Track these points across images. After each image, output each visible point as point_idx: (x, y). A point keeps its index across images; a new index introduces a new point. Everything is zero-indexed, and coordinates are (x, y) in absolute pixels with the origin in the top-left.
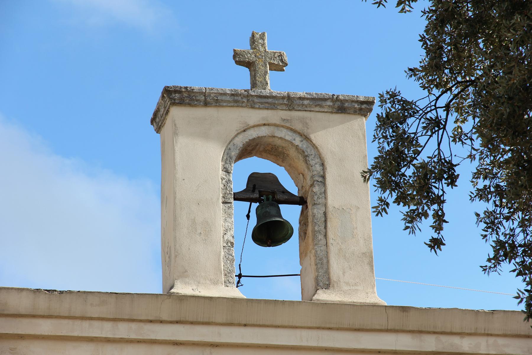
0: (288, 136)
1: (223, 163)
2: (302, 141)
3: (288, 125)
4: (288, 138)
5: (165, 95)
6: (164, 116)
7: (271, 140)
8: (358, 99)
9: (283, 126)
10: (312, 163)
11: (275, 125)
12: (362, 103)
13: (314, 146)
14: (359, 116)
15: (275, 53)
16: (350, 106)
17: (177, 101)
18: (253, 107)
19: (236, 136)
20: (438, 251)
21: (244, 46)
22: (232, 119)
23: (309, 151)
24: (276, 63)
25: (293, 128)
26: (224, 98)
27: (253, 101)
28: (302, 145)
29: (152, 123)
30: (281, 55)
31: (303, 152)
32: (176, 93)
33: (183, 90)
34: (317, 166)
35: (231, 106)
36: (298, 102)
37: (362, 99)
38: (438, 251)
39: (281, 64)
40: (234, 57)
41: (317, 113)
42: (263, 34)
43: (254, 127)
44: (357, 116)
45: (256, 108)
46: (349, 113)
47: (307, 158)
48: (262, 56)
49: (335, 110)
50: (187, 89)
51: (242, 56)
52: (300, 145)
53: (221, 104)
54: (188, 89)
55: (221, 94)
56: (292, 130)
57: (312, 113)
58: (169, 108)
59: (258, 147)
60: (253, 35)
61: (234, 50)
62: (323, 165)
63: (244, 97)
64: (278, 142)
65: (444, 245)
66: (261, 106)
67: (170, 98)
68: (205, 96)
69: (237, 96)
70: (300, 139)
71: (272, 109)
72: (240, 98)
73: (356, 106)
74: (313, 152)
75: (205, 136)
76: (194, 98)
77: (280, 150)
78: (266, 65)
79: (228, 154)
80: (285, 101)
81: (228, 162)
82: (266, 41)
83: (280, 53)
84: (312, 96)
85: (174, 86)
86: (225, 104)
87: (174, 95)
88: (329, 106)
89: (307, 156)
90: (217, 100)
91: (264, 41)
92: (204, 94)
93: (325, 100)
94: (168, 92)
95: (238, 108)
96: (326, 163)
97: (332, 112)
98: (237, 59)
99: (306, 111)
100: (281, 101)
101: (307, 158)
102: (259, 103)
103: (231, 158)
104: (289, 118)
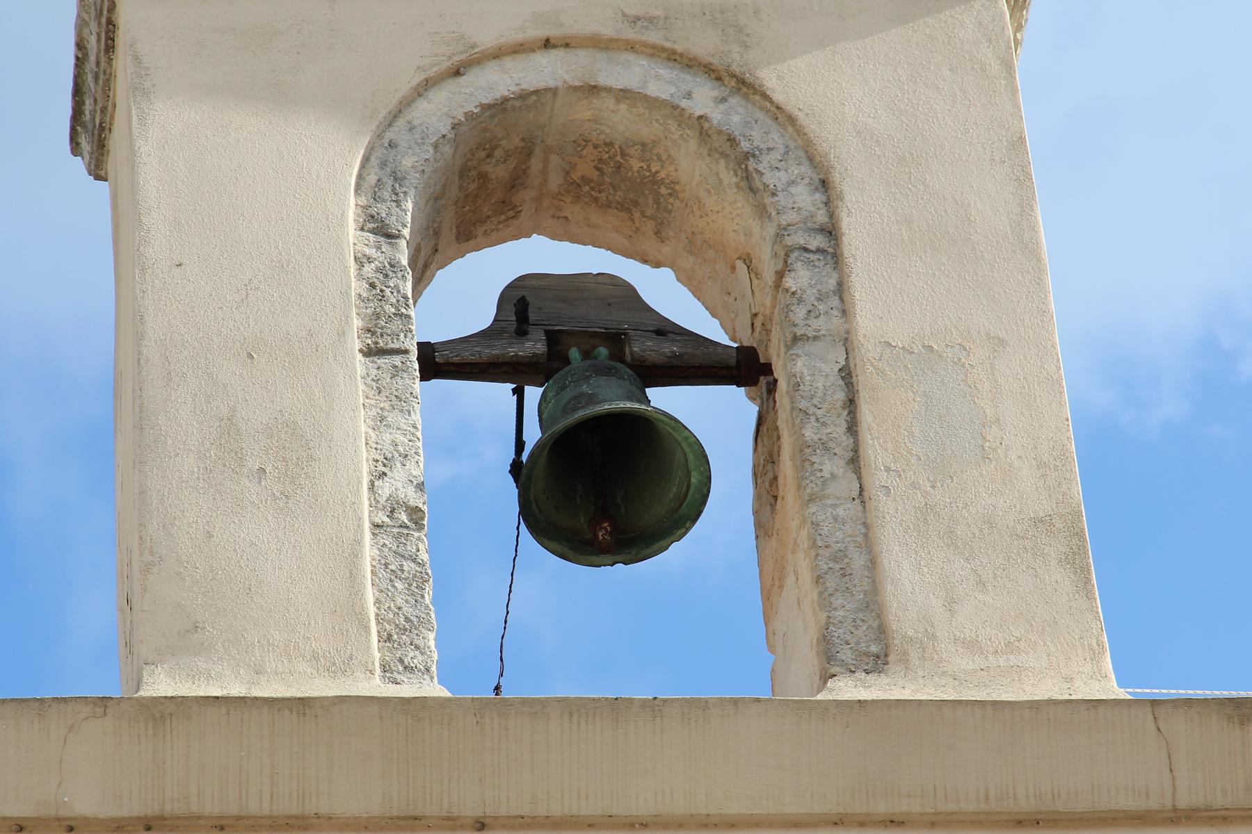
0: (661, 82)
1: (363, 201)
2: (723, 100)
4: (654, 89)
6: (103, 59)
7: (583, 112)
11: (598, 43)
13: (780, 115)
23: (756, 134)
25: (680, 48)
29: (75, 149)
31: (732, 140)
43: (498, 54)
56: (673, 57)
59: (535, 164)
62: (824, 185)
64: (621, 123)
70: (716, 93)
74: (776, 138)
77: (636, 164)
79: (383, 164)
81: (386, 194)
89: (747, 156)
96: (836, 177)
101: (752, 164)
103: (398, 178)
104: (659, 12)
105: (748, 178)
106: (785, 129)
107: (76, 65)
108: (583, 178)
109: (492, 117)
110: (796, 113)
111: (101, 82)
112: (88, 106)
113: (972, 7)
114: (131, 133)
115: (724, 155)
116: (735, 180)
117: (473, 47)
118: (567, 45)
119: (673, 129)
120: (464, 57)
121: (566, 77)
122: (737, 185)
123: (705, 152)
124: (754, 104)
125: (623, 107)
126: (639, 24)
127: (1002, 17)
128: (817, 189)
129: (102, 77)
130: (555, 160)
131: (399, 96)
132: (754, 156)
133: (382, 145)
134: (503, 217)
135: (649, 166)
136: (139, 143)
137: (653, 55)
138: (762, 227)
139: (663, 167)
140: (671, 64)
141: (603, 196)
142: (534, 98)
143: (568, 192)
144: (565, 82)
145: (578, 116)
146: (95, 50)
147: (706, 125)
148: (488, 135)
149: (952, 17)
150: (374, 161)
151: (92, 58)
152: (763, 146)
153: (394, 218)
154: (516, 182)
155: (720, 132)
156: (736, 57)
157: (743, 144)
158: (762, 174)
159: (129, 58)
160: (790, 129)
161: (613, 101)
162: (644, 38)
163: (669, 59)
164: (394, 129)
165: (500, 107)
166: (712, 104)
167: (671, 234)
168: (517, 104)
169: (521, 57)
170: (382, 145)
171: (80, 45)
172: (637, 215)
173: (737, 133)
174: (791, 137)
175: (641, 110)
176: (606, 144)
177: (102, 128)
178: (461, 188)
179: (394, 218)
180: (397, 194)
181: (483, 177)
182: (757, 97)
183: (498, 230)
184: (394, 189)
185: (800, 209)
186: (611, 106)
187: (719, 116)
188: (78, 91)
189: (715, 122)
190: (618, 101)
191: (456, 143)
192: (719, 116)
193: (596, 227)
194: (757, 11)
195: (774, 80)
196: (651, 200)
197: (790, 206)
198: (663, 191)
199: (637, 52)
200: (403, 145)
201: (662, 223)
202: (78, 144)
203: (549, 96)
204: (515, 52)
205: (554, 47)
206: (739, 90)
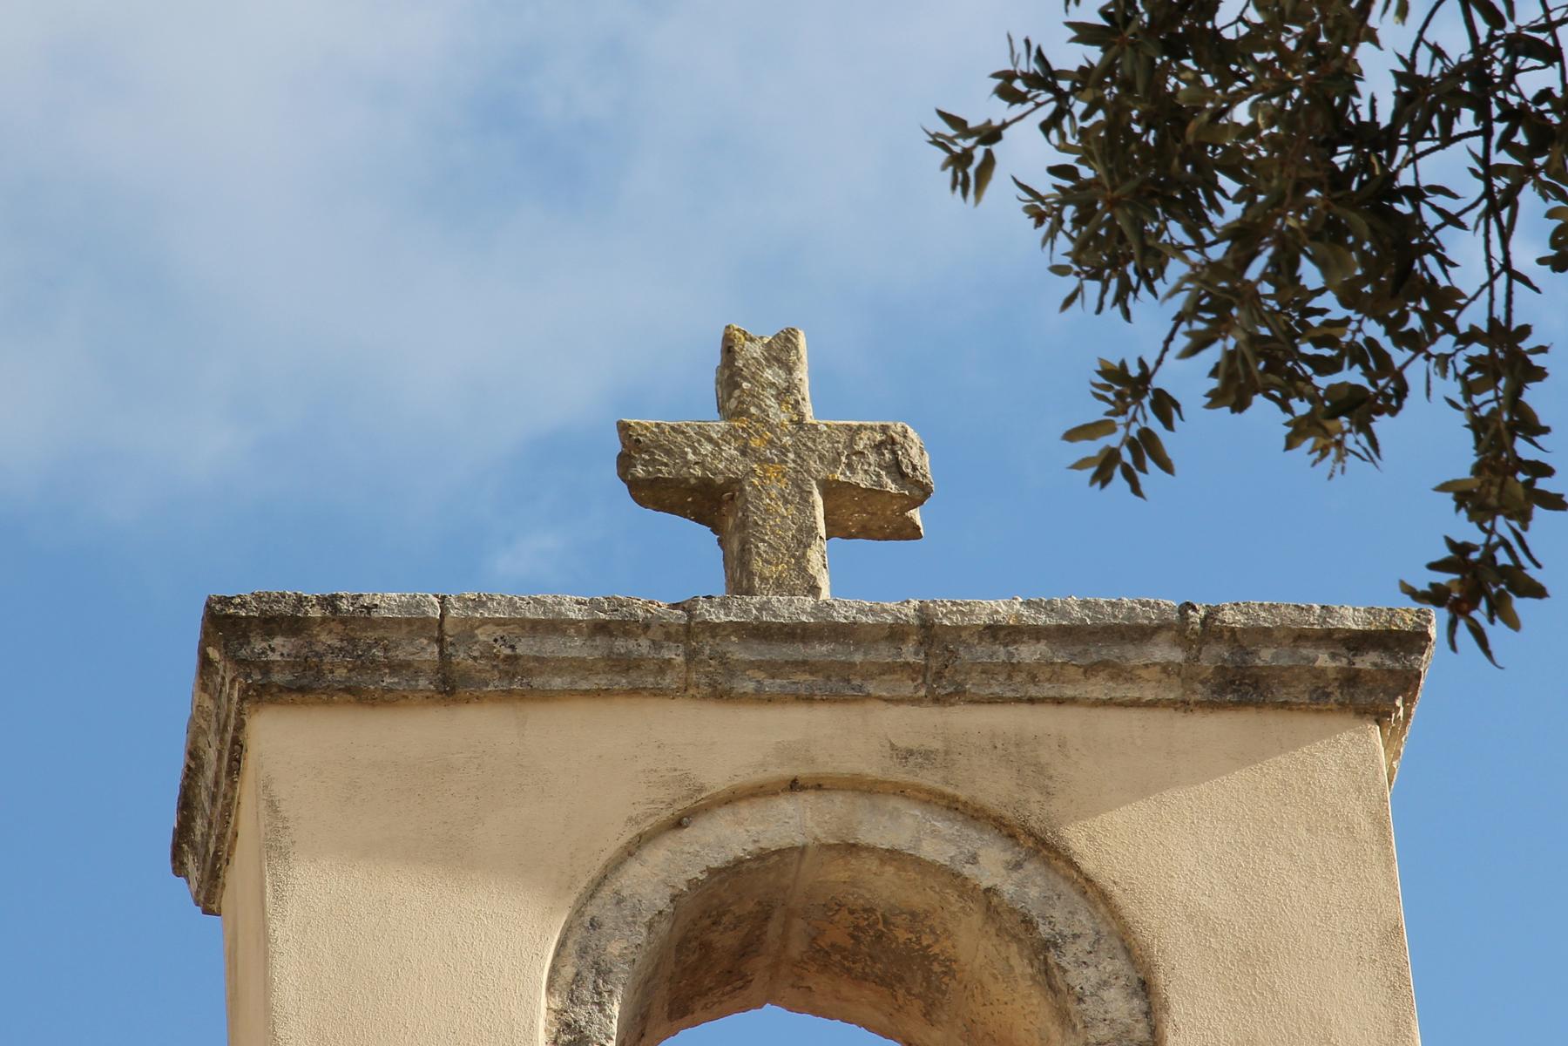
0: (939, 841)
1: (557, 1003)
2: (1018, 866)
3: (930, 779)
4: (930, 850)
5: (214, 654)
6: (224, 782)
7: (838, 873)
8: (1333, 623)
9: (901, 791)
10: (1081, 979)
11: (860, 786)
12: (1358, 642)
13: (1091, 891)
14: (1348, 719)
15: (854, 432)
16: (1285, 662)
17: (277, 677)
18: (721, 695)
19: (632, 850)
20: (1497, 632)
21: (682, 399)
22: (605, 761)
23: (1058, 915)
24: (862, 480)
25: (963, 795)
26: (551, 647)
27: (723, 661)
28: (1021, 885)
29: (179, 867)
30: (888, 443)
31: (1028, 923)
32: (270, 634)
33: (315, 613)
34: (1111, 994)
35: (598, 693)
36: (982, 651)
37: (1352, 619)
38: (1497, 632)
39: (892, 487)
40: (625, 463)
41: (1099, 712)
42: (787, 339)
43: (732, 798)
44: (1334, 721)
45: (743, 699)
46: (1286, 705)
47: (1053, 957)
48: (784, 450)
49: (1201, 692)
50: (336, 609)
51: (668, 452)
52: (1008, 889)
53: (537, 682)
54: (344, 605)
55: (535, 627)
56: (953, 806)
57: (1068, 712)
58: (240, 726)
59: (773, 929)
60: (729, 349)
61: (624, 428)
62: (1145, 988)
63: (668, 636)
64: (885, 887)
65: (1538, 592)
66: (772, 685)
67: (241, 662)
68: (440, 641)
69: (627, 634)
70: (1008, 856)
71: (833, 699)
72: (645, 643)
73: (1323, 660)
74: (1084, 922)
75: (451, 853)
76: (377, 652)
77: (902, 935)
78: (805, 496)
79: (583, 952)
80: (909, 653)
81: (586, 994)
82: (802, 374)
83: (884, 429)
84: (1065, 614)
85: (258, 598)
86: (557, 683)
87: (259, 645)
88: (1165, 668)
89: (1047, 945)
90: (513, 659)
91: (790, 370)
92: (436, 630)
93: (1140, 634)
94: (225, 625)
95: (635, 700)
96: (1161, 979)
97: (1183, 705)
98: (640, 471)
99: (1032, 701)
100: (884, 654)
101: (1053, 957)
102: (758, 665)
103: (602, 972)
104: (937, 745)
105: (1047, 971)
106: (1096, 908)
107: (187, 776)
108: (833, 945)
109: (721, 882)
110: (1110, 887)
111: (219, 806)
112: (199, 826)
113: (1337, 741)
114: (263, 909)
115: (1016, 938)
116: (1029, 970)
117: (700, 790)
118: (819, 787)
119: (952, 900)
120: (688, 804)
121: (818, 831)
122: (1033, 978)
123: (993, 931)
124: (1056, 871)
125: (890, 870)
126: (912, 760)
127: (1375, 759)
128: (1135, 993)
129: (220, 801)
130: (799, 925)
131: (604, 857)
132: (1056, 945)
133: (581, 924)
134: (728, 988)
135: (919, 939)
136: (274, 924)
137: (928, 802)
138: (1063, 1035)
139: (937, 941)
140: (951, 815)
141: (858, 967)
142: (776, 858)
143: (813, 960)
144: (816, 839)
145: (832, 878)
146: (214, 767)
147: (995, 900)
148: (715, 901)
149: (1313, 755)
150: (572, 947)
151: (210, 774)
152: (1067, 932)
153: (596, 1027)
154: (748, 948)
155: (1013, 911)
156: (1035, 807)
157: (1041, 928)
158: (1065, 971)
159: (263, 804)
160: (1102, 908)
161: (877, 862)
162: (917, 780)
163: (948, 808)
164: (597, 901)
165: (735, 869)
166: (1003, 872)
167: (945, 1018)
168: (754, 865)
169: (760, 802)
170: (581, 924)
171: (194, 754)
172: (901, 992)
173: (1034, 913)
174: (1104, 919)
175: (912, 875)
176: (865, 910)
177: (216, 857)
178: (677, 963)
179: (596, 1027)
180: (600, 994)
181: (706, 947)
182: (1061, 864)
183: (721, 1002)
184: (596, 986)
185: (1113, 1021)
186: (874, 868)
187: (1012, 889)
188: (186, 805)
189: (1007, 897)
190: (883, 862)
191: (675, 916)
192: (1012, 889)
193: (847, 1000)
194: (1062, 745)
195: (1083, 841)
196: (919, 977)
197: (1101, 1016)
198: (936, 967)
199: (908, 798)
200: (609, 924)
201: (932, 1005)
202: (182, 864)
203: (796, 855)
204: (753, 795)
205: (803, 788)
206: (1038, 852)
